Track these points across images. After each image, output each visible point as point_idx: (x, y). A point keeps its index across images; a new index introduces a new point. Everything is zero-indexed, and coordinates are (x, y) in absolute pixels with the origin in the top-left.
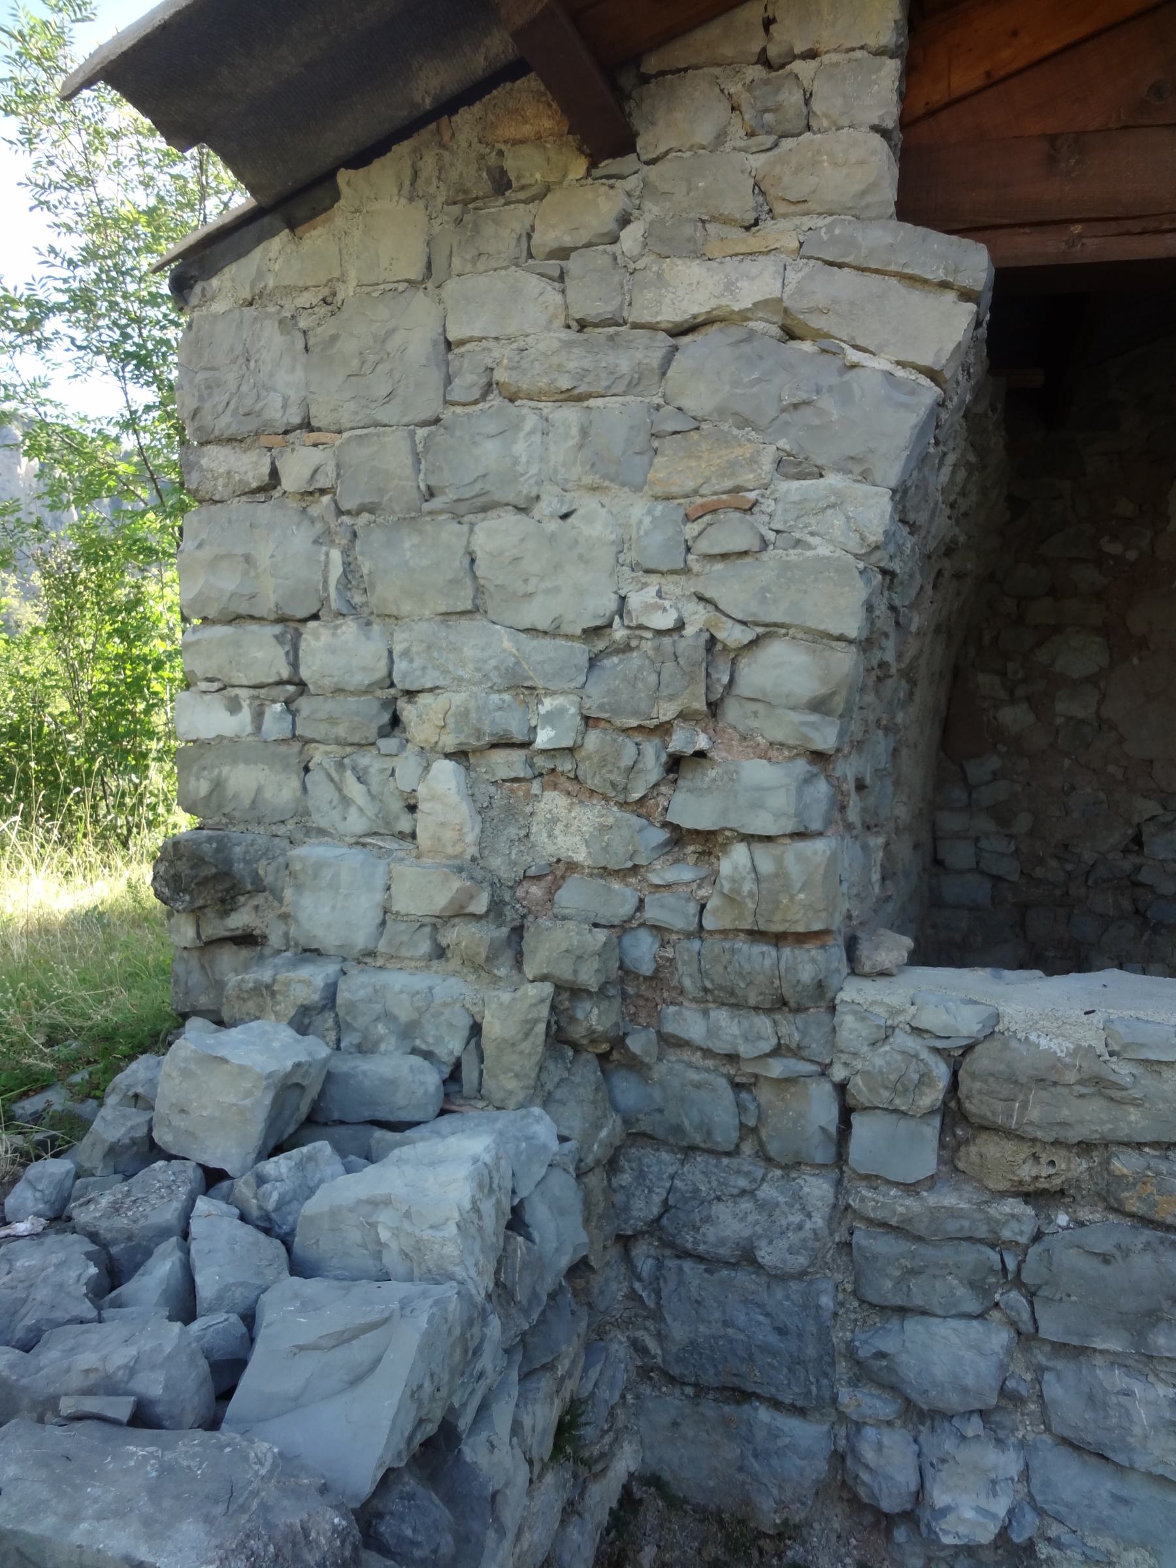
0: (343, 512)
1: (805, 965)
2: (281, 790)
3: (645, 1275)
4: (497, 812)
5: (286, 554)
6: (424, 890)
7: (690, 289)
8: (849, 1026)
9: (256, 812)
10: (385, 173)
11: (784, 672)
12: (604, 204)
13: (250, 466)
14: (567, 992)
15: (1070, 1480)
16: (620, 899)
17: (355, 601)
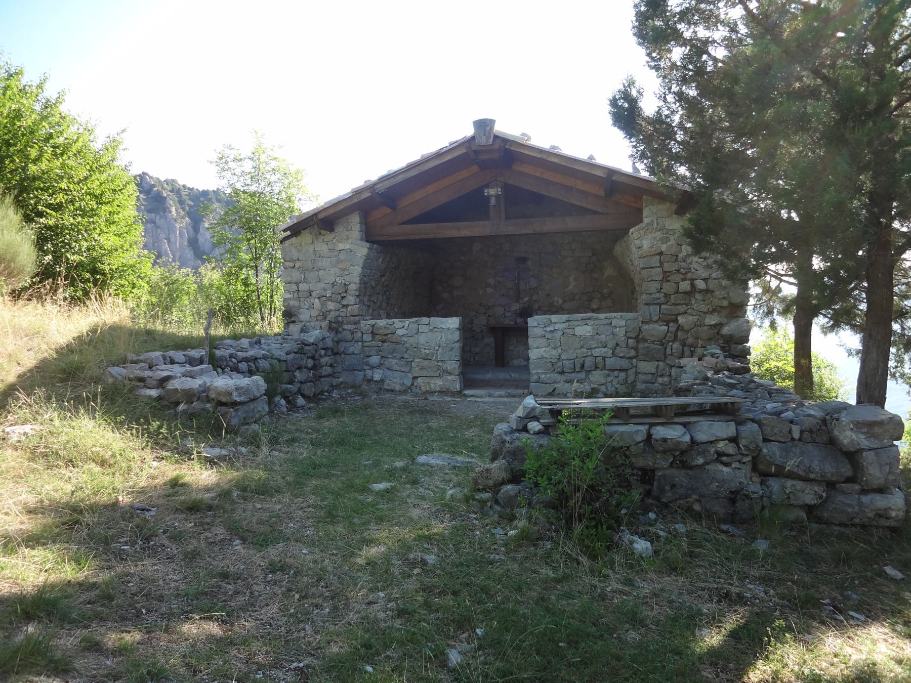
0: (304, 270)
1: (357, 318)
2: (296, 303)
3: (240, 365)
4: (323, 304)
5: (296, 275)
6: (315, 313)
7: (341, 246)
8: (362, 325)
9: (294, 307)
10: (307, 231)
11: (352, 287)
12: (331, 237)
13: (292, 264)
14: (330, 322)
15: (389, 373)
16: (337, 313)
17: (305, 280)
